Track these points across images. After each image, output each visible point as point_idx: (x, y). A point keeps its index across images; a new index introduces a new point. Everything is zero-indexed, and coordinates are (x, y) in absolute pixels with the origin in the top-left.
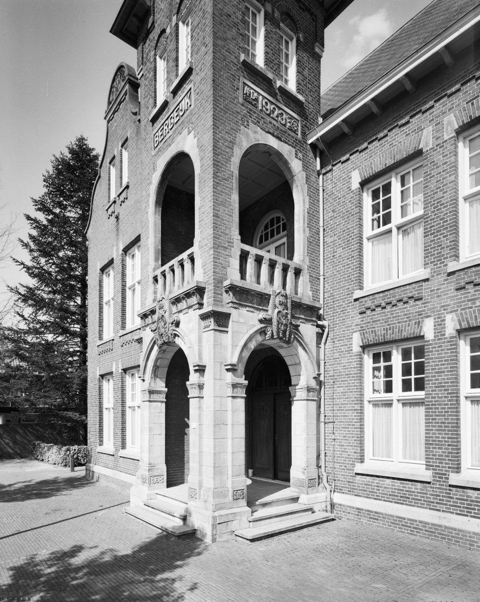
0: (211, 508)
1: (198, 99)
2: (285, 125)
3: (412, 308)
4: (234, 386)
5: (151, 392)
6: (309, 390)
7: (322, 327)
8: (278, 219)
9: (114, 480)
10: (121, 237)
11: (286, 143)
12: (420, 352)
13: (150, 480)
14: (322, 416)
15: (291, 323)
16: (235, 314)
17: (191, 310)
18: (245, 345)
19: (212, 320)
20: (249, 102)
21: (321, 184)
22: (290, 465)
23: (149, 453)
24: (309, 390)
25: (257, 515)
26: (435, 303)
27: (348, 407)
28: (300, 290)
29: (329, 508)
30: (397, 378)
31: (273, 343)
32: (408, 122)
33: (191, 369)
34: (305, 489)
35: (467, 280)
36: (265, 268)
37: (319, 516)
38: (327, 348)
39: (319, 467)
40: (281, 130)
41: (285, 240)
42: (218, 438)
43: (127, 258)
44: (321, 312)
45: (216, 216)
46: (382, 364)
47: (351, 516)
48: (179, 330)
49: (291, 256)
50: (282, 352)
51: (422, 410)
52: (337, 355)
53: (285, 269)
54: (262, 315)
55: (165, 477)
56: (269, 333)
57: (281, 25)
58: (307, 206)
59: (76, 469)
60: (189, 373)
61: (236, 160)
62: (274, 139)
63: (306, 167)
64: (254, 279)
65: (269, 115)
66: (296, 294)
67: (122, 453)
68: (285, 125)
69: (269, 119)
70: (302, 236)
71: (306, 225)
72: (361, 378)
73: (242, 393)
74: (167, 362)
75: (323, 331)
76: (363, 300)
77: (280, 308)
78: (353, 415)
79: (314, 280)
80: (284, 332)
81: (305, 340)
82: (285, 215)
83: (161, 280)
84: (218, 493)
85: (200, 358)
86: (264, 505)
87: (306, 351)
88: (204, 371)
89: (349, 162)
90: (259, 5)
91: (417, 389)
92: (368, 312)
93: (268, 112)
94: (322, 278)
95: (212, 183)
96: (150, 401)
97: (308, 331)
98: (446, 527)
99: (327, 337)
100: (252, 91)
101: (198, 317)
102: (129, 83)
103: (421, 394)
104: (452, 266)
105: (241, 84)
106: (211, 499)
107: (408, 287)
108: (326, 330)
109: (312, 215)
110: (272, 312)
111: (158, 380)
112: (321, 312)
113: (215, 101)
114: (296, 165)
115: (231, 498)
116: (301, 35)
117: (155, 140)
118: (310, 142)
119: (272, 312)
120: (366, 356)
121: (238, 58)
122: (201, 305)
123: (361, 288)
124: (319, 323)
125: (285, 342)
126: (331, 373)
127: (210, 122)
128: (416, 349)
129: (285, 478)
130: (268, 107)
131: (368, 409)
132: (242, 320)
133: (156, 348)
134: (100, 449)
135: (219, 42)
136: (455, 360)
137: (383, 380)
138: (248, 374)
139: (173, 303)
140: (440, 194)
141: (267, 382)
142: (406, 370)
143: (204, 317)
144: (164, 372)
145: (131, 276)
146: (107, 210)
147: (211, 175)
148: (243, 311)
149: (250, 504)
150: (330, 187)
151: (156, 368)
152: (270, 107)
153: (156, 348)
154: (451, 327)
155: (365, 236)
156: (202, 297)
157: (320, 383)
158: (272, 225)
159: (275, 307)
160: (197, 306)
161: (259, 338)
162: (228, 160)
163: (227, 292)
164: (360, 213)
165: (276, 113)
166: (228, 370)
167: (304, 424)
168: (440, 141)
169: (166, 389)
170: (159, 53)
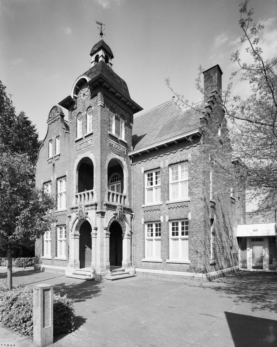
0: (100, 271)
1: (95, 141)
2: (121, 151)
3: (158, 212)
4: (107, 234)
5: (75, 235)
6: (128, 235)
7: (132, 215)
8: (118, 176)
9: (51, 269)
10: (55, 173)
11: (122, 156)
12: (160, 225)
13: (75, 266)
14: (132, 244)
15: (123, 214)
16: (107, 212)
17: (92, 210)
18: (110, 222)
19: (100, 214)
20: (111, 146)
21: (132, 168)
22: (122, 259)
23: (74, 256)
24: (128, 235)
25: (113, 274)
26: (163, 212)
27: (140, 241)
28: (126, 203)
29: (134, 273)
30: (154, 232)
31: (117, 220)
32: (157, 158)
33: (93, 228)
34: (127, 267)
35: (171, 207)
36: (115, 197)
37: (131, 275)
38: (134, 221)
39: (131, 260)
40: (120, 153)
41: (120, 183)
42: (102, 250)
43: (58, 181)
44: (132, 210)
45: (101, 182)
46: (150, 228)
47: (141, 275)
48: (88, 215)
49: (122, 192)
50: (120, 223)
51: (160, 242)
52: (137, 224)
53: (121, 196)
54: (114, 212)
55: (79, 265)
56: (116, 218)
57: (120, 119)
58: (128, 176)
59: (26, 267)
60: (91, 230)
61: (107, 164)
62: (118, 156)
63: (127, 163)
64: (112, 201)
65: (116, 149)
66: (124, 204)
67: (56, 258)
68: (121, 151)
69: (116, 150)
70: (126, 186)
71: (127, 182)
72: (144, 232)
73: (108, 236)
74: (80, 225)
75: (133, 216)
76: (145, 208)
77: (120, 210)
78: (142, 243)
79: (130, 199)
80: (121, 217)
81: (127, 220)
82: (120, 174)
83: (79, 197)
84: (102, 267)
85: (96, 225)
86: (115, 271)
87: (127, 223)
88: (97, 229)
89: (140, 164)
90: (114, 114)
91: (176, 235)
92: (146, 212)
93: (116, 148)
94: (132, 199)
95: (100, 172)
96: (74, 238)
97: (128, 216)
98: (165, 274)
99: (134, 218)
100: (111, 142)
101: (95, 213)
102: (60, 115)
103: (187, 237)
104: (167, 202)
105: (108, 141)
106: (100, 269)
107: (157, 206)
108: (134, 216)
109: (129, 178)
110: (117, 211)
111: (77, 231)
112: (132, 210)
113: (101, 147)
114: (124, 163)
115: (105, 268)
116: (126, 121)
117: (77, 148)
118: (129, 155)
119: (117, 211)
120: (145, 225)
121: (107, 133)
122: (96, 209)
123: (144, 204)
124: (131, 213)
125: (121, 220)
126: (135, 230)
127: (99, 153)
128: (159, 225)
129: (120, 265)
130: (116, 146)
131: (146, 241)
132: (108, 214)
133: (78, 220)
134: (42, 257)
135: (102, 129)
136: (168, 228)
137: (150, 233)
138: (110, 231)
139: (86, 207)
140: (165, 181)
141: (116, 232)
142: (157, 230)
143: (97, 213)
144: (79, 228)
145: (60, 189)
146: (48, 160)
147: (100, 170)
148: (109, 211)
149: (111, 271)
150: (135, 170)
151: (77, 227)
152: (117, 146)
153: (78, 220)
154: (167, 219)
155: (145, 188)
156: (96, 206)
157: (132, 233)
158: (116, 177)
159: (118, 209)
160: (95, 209)
161: (114, 219)
162: (105, 165)
163: (104, 205)
164: (144, 180)
165: (118, 148)
166: (104, 229)
167: (127, 246)
168: (165, 167)
169: (80, 234)
170: (78, 118)
